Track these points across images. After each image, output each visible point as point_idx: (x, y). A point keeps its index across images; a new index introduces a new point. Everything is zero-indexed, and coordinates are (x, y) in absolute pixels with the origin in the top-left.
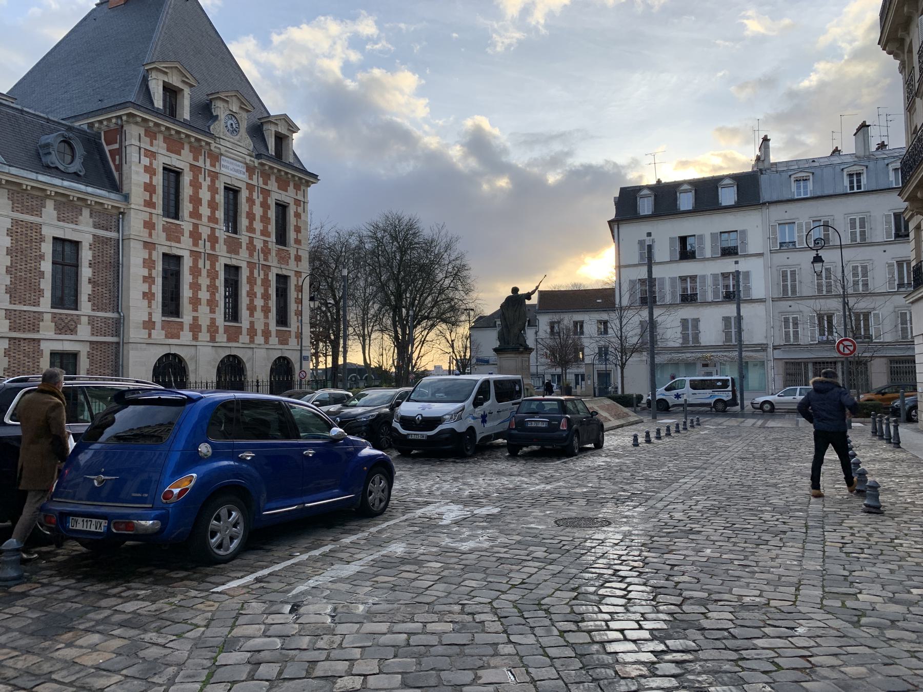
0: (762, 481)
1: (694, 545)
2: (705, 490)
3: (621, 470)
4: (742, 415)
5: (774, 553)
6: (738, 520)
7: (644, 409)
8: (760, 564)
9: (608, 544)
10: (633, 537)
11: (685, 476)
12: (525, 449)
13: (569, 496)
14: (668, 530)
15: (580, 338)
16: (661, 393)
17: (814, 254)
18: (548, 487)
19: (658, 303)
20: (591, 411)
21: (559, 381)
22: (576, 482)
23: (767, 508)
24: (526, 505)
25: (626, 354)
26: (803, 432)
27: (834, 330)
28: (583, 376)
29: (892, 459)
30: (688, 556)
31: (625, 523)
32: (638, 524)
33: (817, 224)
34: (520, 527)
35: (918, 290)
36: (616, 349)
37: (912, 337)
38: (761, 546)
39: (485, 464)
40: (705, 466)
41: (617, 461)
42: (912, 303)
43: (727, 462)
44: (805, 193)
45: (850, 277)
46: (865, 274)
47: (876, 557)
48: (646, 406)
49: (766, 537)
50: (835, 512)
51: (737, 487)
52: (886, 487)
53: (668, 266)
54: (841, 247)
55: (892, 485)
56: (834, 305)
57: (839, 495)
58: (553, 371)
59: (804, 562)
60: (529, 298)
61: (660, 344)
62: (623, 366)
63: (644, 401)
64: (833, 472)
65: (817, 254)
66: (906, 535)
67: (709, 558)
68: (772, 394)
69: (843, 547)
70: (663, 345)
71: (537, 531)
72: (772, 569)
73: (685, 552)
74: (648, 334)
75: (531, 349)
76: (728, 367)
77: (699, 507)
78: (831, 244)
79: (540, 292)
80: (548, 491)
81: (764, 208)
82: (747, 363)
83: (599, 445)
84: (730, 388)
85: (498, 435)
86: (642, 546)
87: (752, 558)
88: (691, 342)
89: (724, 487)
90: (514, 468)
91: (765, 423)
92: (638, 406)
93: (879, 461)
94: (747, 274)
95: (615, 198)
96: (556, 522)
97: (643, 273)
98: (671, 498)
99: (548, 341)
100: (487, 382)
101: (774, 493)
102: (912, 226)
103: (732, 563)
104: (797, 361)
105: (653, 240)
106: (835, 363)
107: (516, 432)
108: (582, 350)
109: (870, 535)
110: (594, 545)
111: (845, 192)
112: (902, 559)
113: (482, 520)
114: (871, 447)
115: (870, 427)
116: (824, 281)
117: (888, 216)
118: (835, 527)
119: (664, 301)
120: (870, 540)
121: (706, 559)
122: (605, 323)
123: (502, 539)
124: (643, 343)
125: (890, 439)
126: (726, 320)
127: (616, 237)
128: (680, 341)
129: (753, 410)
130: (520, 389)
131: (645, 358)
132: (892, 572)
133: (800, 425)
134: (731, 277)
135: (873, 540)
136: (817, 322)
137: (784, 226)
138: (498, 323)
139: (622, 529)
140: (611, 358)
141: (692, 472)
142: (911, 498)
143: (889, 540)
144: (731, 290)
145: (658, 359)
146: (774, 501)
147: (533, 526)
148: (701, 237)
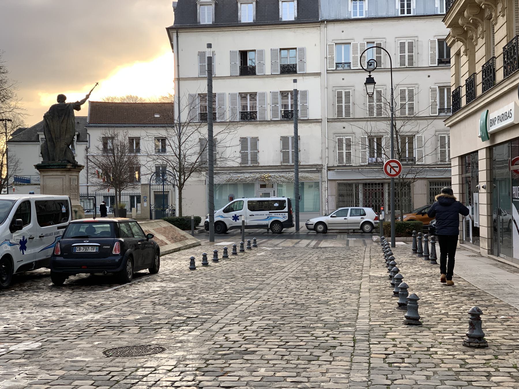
0: (315, 299)
1: (249, 365)
2: (261, 309)
3: (177, 295)
4: (297, 236)
5: (324, 369)
6: (292, 338)
7: (201, 232)
8: (312, 379)
9: (160, 371)
10: (187, 362)
11: (241, 297)
12: (72, 278)
13: (120, 324)
14: (224, 352)
15: (136, 156)
16: (219, 215)
17: (366, 75)
18: (97, 317)
19: (218, 120)
20: (146, 234)
21: (112, 202)
22: (129, 309)
23: (319, 325)
24: (71, 337)
25: (184, 173)
26: (352, 251)
27: (383, 152)
28: (139, 198)
29: (429, 274)
30: (242, 377)
31: (180, 348)
32: (192, 348)
33: (372, 45)
34: (63, 361)
35: (456, 114)
36: (174, 168)
37: (450, 160)
38: (312, 362)
39: (24, 296)
40: (261, 286)
41: (173, 285)
42: (451, 126)
43: (282, 282)
44: (361, 13)
45: (398, 100)
46: (411, 98)
47: (415, 365)
48: (203, 228)
49: (317, 352)
50: (380, 325)
51: (291, 306)
52: (424, 301)
53: (228, 81)
54: (391, 70)
55: (429, 298)
56: (383, 127)
57: (384, 309)
58: (106, 192)
59: (352, 374)
60: (78, 109)
61: (219, 164)
62: (181, 187)
63: (202, 223)
64: (378, 288)
65: (370, 76)
66: (440, 343)
67: (263, 377)
68: (326, 215)
69: (386, 358)
70: (222, 164)
71: (83, 364)
72: (322, 384)
73: (240, 373)
74: (207, 152)
75: (80, 166)
76: (284, 189)
77: (254, 328)
78: (382, 67)
79: (92, 104)
80: (97, 321)
81: (323, 26)
82: (303, 184)
83: (154, 270)
84: (286, 209)
85: (40, 264)
86: (196, 370)
87: (304, 374)
88: (249, 162)
89: (278, 306)
90: (58, 299)
91: (318, 244)
92: (195, 229)
93: (418, 276)
94: (305, 94)
95: (174, 3)
96: (104, 353)
97: (202, 87)
98: (227, 319)
99: (101, 159)
100: (26, 203)
101: (325, 310)
102: (453, 52)
103: (285, 380)
104: (349, 182)
105: (213, 52)
106: (382, 184)
107: (61, 259)
108: (138, 169)
109: (410, 345)
110: (145, 373)
111: (396, 15)
112: (436, 365)
113: (19, 356)
114: (412, 264)
115: (411, 245)
116: (375, 103)
117: (432, 42)
118: (379, 340)
119: (223, 118)
120: (409, 350)
121: (260, 378)
122: (163, 140)
123: (44, 375)
124: (202, 162)
125: (428, 256)
126: (284, 140)
127: (174, 45)
128: (239, 160)
129: (308, 231)
130: (67, 211)
131: (203, 178)
132: (428, 377)
133: (350, 245)
134: (290, 96)
135: (412, 349)
136: (367, 143)
137: (340, 46)
138: (42, 136)
139: (176, 354)
140: (169, 178)
141: (248, 293)
142: (446, 310)
143: (426, 349)
144: (290, 109)
145: (217, 180)
146: (326, 317)
147: (78, 358)
148: (261, 52)
